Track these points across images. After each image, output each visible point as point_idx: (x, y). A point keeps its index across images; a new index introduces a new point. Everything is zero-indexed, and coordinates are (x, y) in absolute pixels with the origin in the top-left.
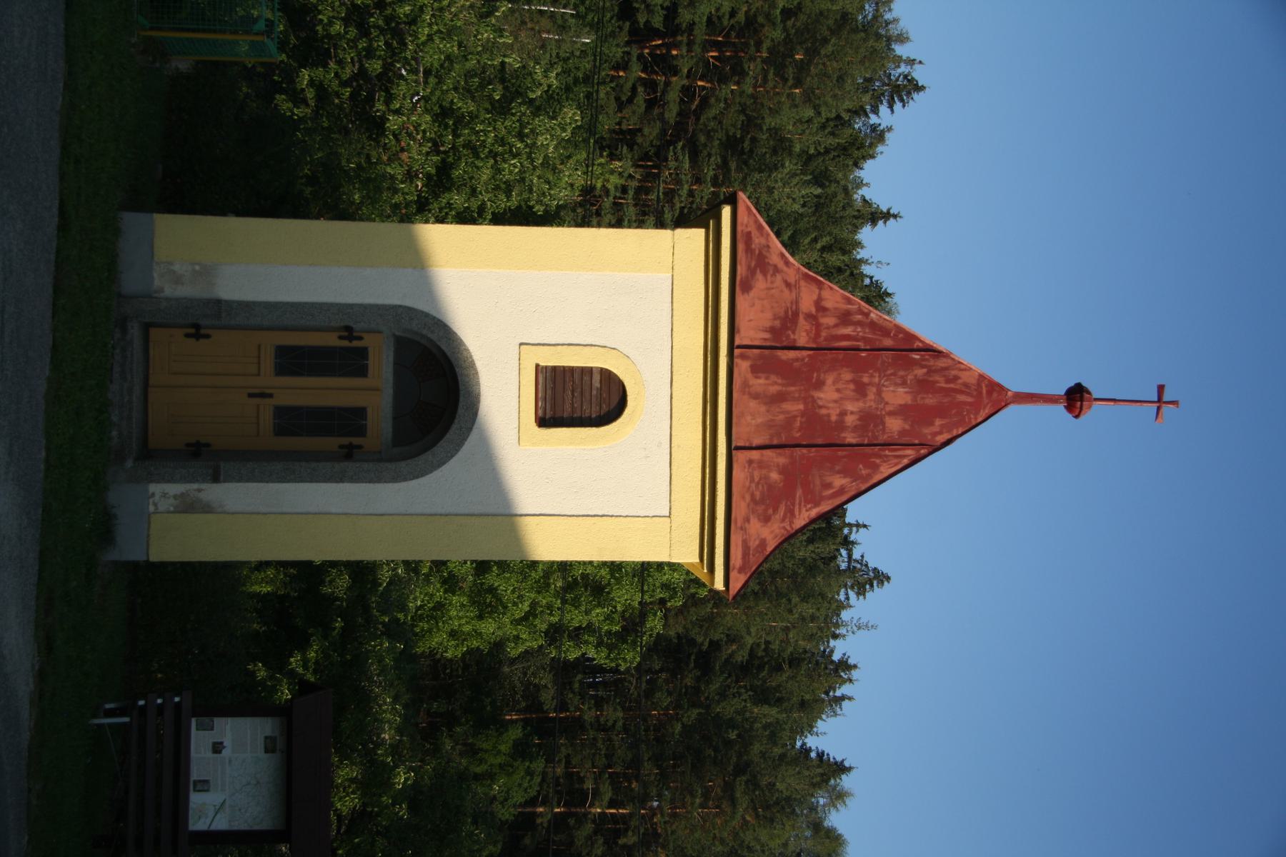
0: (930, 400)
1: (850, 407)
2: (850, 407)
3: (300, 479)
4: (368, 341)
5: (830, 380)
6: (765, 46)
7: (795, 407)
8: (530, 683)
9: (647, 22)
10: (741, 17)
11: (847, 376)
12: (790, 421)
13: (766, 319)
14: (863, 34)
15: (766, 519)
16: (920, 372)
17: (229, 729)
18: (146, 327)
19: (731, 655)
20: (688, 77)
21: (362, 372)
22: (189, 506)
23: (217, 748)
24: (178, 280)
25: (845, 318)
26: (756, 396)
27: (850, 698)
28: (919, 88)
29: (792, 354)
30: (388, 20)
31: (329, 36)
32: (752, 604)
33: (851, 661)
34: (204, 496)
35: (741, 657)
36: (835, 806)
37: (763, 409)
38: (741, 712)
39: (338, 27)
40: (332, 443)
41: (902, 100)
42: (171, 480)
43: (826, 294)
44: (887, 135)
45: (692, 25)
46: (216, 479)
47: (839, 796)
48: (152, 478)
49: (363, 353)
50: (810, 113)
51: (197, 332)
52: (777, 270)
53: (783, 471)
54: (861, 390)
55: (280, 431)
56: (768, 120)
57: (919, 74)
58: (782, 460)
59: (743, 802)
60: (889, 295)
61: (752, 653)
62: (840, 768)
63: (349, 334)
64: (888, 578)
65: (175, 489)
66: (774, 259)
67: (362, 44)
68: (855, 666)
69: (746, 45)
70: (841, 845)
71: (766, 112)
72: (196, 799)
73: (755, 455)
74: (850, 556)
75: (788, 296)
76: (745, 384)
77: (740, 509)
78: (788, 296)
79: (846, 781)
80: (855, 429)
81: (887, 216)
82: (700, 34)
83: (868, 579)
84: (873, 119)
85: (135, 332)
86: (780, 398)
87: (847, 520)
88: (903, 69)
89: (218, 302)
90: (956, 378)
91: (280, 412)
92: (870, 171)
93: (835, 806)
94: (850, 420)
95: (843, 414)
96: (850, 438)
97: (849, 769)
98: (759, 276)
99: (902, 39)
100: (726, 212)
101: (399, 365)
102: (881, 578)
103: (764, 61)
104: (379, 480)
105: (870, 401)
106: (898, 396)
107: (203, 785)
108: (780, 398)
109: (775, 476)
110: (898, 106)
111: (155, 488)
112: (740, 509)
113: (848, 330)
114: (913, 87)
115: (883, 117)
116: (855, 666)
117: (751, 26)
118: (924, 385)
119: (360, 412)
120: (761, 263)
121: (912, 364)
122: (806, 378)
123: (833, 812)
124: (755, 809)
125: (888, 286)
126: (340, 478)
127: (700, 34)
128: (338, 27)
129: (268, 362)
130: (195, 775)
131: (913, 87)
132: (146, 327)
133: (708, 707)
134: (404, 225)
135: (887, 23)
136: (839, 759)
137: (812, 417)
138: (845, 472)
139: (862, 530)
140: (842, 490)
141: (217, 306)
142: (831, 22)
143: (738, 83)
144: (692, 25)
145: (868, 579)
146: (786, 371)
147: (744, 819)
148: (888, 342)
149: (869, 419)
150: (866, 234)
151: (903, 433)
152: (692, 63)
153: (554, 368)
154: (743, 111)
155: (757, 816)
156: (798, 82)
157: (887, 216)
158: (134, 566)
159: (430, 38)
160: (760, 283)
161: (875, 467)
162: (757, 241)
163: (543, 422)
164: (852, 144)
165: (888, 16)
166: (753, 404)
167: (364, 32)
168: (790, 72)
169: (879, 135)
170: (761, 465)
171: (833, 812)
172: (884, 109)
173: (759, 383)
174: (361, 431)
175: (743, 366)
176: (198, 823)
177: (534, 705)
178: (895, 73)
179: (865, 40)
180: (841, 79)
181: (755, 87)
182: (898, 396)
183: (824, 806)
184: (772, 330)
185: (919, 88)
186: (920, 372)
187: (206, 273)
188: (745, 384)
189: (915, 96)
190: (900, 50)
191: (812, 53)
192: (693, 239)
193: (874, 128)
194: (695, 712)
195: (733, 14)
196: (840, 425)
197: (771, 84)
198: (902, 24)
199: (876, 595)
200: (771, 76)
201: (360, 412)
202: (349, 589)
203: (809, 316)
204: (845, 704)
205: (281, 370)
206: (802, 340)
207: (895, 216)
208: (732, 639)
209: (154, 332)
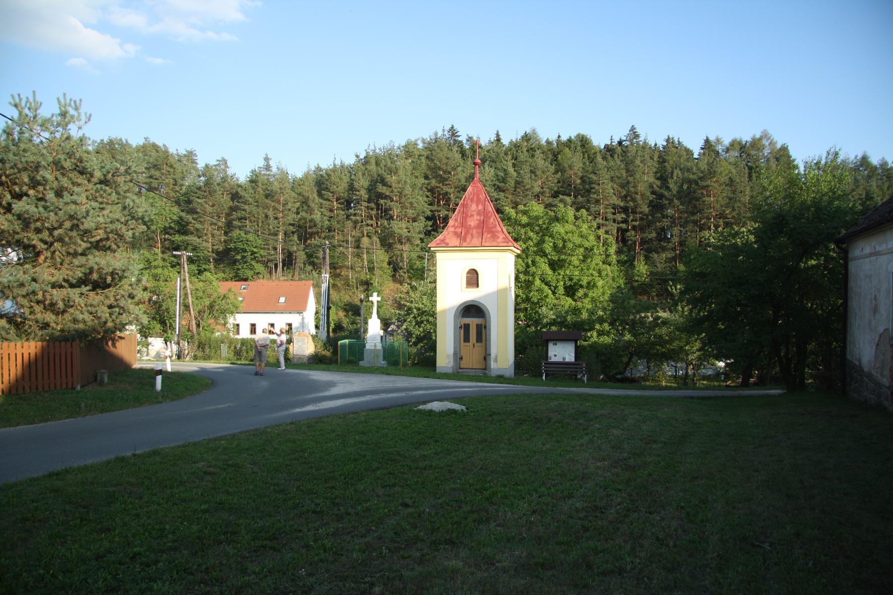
0: (475, 199)
1: (475, 218)
2: (475, 218)
3: (490, 338)
4: (462, 324)
5: (469, 223)
6: (438, 185)
7: (475, 231)
8: (665, 261)
9: (431, 226)
10: (429, 194)
11: (468, 219)
12: (477, 232)
13: (455, 239)
14: (433, 152)
15: (498, 237)
16: (469, 201)
17: (551, 353)
18: (460, 368)
19: (657, 186)
20: (449, 211)
21: (469, 325)
22: (496, 360)
23: (555, 356)
24: (450, 362)
25: (456, 220)
26: (471, 241)
27: (679, 139)
28: (453, 127)
29: (463, 232)
30: (419, 316)
31: (424, 331)
32: (636, 180)
33: (667, 138)
34: (494, 357)
35: (658, 183)
36: (722, 142)
37: (474, 239)
38: (676, 183)
39: (421, 329)
40: (484, 331)
41: (457, 133)
42: (490, 364)
43: (451, 225)
44: (470, 136)
45: (431, 211)
46: (490, 355)
47: (718, 141)
48: (490, 368)
49: (465, 325)
50: (460, 169)
51: (461, 358)
52: (445, 237)
53: (488, 234)
54: (472, 216)
55: (481, 341)
56: (462, 183)
57: (448, 127)
58: (486, 234)
59: (708, 182)
60: (526, 133)
61: (657, 179)
62: (707, 141)
63: (461, 327)
64: (633, 126)
65: (492, 363)
66: (442, 238)
67: (425, 323)
68: (668, 136)
69: (438, 191)
70: (736, 140)
71: (460, 184)
72: (567, 360)
73: (483, 241)
74: (625, 141)
75: (450, 234)
76: (468, 244)
77: (495, 244)
78: (450, 234)
79: (712, 138)
80: (481, 217)
81: (498, 135)
82: (435, 208)
83: (634, 133)
84: (464, 141)
85: (460, 370)
86: (472, 235)
87: (609, 143)
88: (446, 133)
89: (454, 354)
90: (471, 193)
91: (477, 341)
92: (484, 142)
93: (722, 142)
94: (478, 218)
95: (477, 220)
96: (482, 218)
97: (707, 137)
98: (445, 241)
99: (436, 134)
100: (432, 249)
101: (467, 317)
102: (633, 129)
103: (443, 185)
104: (490, 321)
105: (474, 213)
106: (474, 207)
107: (564, 359)
108: (472, 235)
109: (489, 236)
110: (458, 134)
111: (492, 367)
112: (495, 244)
113: (459, 219)
114: (452, 129)
115: (463, 138)
116: (668, 136)
117: (432, 190)
118: (472, 200)
119: (477, 325)
120: (443, 241)
121: (467, 204)
122: (468, 229)
123: (724, 143)
124: (711, 177)
125: (522, 134)
126: (490, 329)
127: (435, 208)
128: (421, 329)
129: (467, 344)
130: (562, 360)
131: (452, 129)
132: (460, 368)
133: (674, 196)
134: (438, 316)
135: (431, 139)
136: (704, 142)
137: (477, 227)
138: (490, 219)
139: (613, 138)
140: (494, 220)
141: (455, 354)
142: (429, 163)
143: (450, 194)
144: (431, 211)
145: (634, 133)
146: (466, 234)
147: (715, 182)
148: (462, 210)
149: (479, 213)
150: (505, 141)
151: (482, 205)
152: (444, 210)
153: (467, 284)
154: (460, 192)
155: (714, 177)
156: (450, 173)
157: (498, 135)
158: (515, 375)
159: (423, 304)
160: (447, 241)
161: (489, 211)
162: (438, 242)
163: (478, 286)
164: (472, 149)
165: (429, 140)
166: (472, 242)
167: (422, 322)
168: (446, 176)
169: (470, 139)
170: (486, 239)
171: (724, 143)
172: (459, 139)
173: (468, 240)
174: (481, 325)
175: (464, 244)
176: (573, 360)
177: (674, 259)
178: (448, 136)
179: (435, 150)
180: (448, 158)
181: (451, 188)
182: (474, 207)
183: (722, 146)
184: (457, 237)
185: (453, 127)
186: (469, 201)
187: (448, 356)
188: (468, 244)
189: (455, 128)
190: (439, 135)
191: (440, 169)
192: (438, 255)
193: (468, 141)
194: (676, 201)
195: (428, 197)
196: (479, 220)
197: (450, 182)
198: (431, 134)
199: (639, 130)
200: (447, 183)
201: (477, 325)
202: (555, 326)
203: (455, 229)
204: (681, 141)
205: (468, 341)
206: (460, 230)
207: (498, 132)
208: (651, 186)
209: (461, 367)
